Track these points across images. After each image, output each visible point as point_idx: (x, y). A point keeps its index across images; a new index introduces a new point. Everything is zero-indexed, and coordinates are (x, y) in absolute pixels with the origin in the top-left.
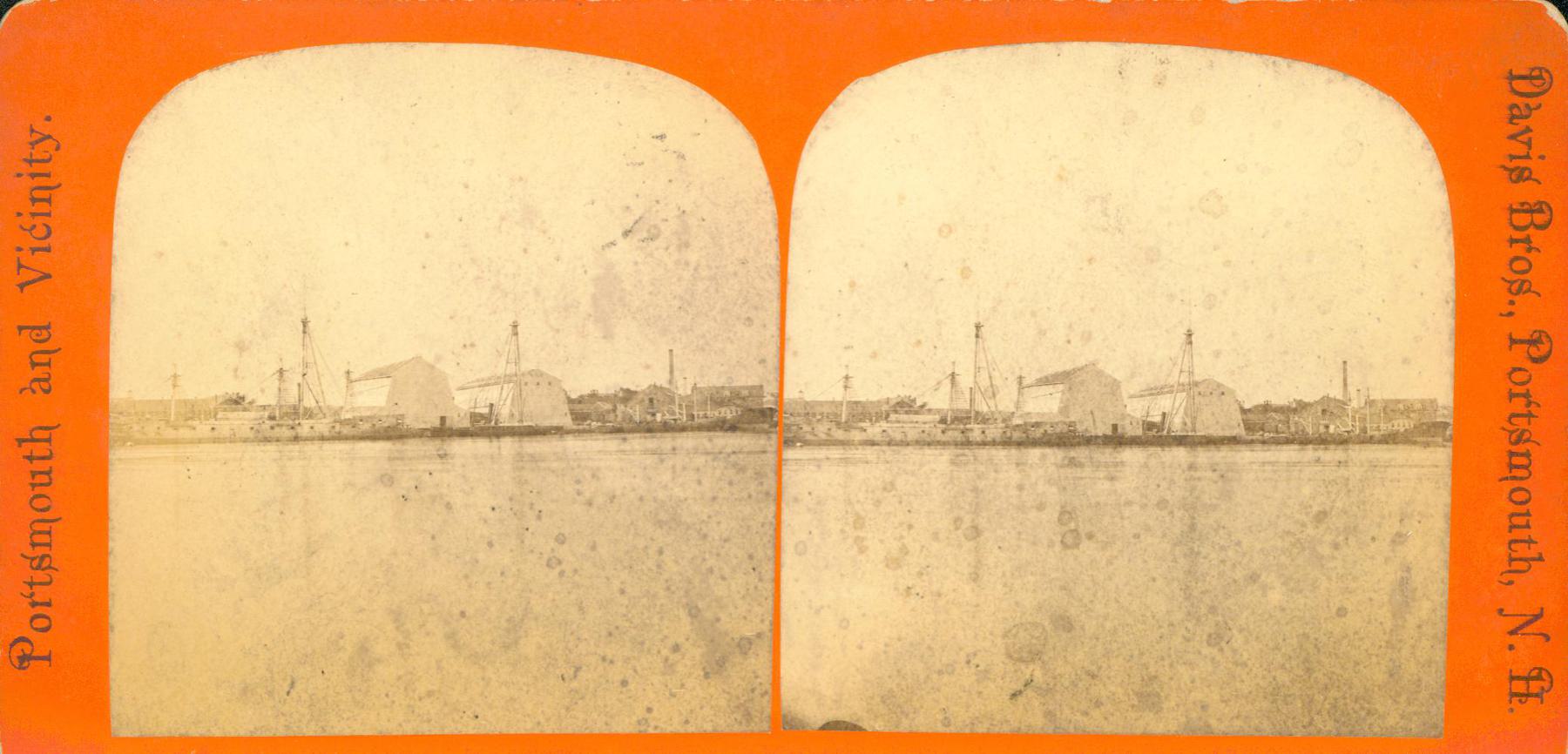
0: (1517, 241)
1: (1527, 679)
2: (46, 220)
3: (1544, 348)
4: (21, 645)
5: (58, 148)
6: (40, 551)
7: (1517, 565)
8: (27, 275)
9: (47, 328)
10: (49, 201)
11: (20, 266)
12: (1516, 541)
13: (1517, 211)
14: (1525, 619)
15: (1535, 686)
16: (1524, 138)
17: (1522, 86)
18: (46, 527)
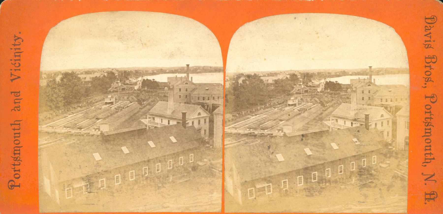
0: (427, 66)
1: (430, 194)
2: (19, 62)
3: (10, 184)
4: (12, 182)
5: (22, 41)
6: (428, 127)
7: (426, 162)
8: (13, 77)
9: (19, 92)
10: (20, 56)
11: (11, 74)
12: (18, 129)
13: (427, 58)
14: (430, 176)
15: (433, 196)
16: (429, 35)
17: (429, 21)
18: (18, 149)
